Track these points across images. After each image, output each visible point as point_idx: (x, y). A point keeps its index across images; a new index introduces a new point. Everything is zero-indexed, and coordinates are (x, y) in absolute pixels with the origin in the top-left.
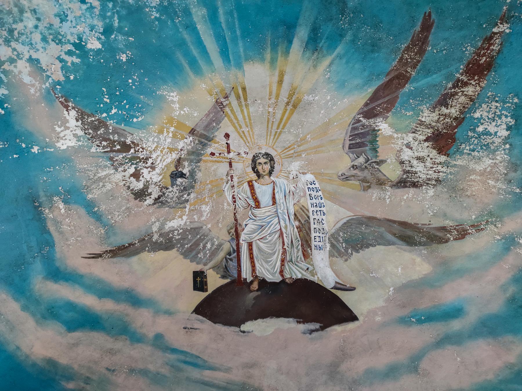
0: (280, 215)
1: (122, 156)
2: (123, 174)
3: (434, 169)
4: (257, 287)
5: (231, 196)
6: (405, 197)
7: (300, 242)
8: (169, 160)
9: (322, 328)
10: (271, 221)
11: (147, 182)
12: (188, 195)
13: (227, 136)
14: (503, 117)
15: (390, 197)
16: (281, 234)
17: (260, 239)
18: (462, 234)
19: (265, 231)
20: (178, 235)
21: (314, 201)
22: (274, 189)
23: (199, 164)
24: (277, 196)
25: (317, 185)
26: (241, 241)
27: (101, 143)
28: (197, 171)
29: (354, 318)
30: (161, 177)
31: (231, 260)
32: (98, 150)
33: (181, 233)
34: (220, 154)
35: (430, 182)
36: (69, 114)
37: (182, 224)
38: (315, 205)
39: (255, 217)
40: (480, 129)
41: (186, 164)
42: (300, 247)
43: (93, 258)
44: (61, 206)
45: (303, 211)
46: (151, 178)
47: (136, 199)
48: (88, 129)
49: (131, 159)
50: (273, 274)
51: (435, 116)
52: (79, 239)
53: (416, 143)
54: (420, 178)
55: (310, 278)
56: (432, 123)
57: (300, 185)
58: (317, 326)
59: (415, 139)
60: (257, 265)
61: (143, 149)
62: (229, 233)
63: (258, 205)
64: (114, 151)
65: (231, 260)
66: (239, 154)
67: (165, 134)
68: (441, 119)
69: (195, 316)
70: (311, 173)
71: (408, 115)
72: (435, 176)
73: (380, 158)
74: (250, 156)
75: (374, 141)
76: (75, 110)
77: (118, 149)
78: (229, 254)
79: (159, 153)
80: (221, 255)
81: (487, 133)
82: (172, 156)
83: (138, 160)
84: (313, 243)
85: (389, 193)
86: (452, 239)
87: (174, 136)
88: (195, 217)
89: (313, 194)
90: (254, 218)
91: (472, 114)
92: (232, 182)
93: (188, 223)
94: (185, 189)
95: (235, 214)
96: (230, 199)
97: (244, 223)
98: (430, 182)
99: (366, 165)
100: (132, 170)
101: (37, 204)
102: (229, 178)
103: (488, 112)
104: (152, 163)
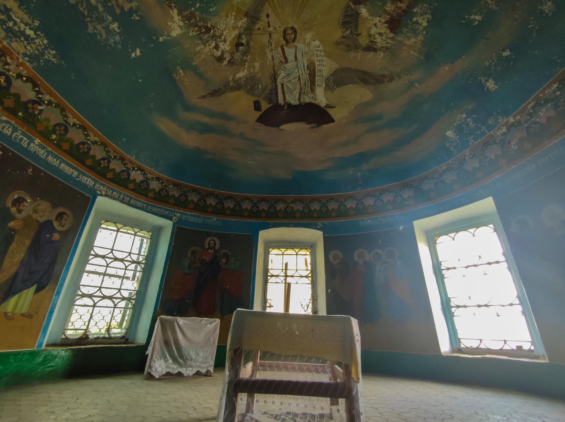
0: (299, 67)
1: (207, 36)
2: (209, 47)
3: (386, 41)
4: (287, 108)
5: (271, 57)
6: (368, 57)
7: (309, 83)
8: (233, 35)
9: (318, 126)
10: (294, 71)
11: (223, 51)
12: (246, 57)
13: (268, 16)
14: (427, 15)
15: (360, 57)
16: (299, 79)
17: (288, 81)
18: (391, 79)
19: (290, 77)
20: (243, 81)
21: (319, 58)
22: (296, 51)
23: (251, 36)
24: (298, 55)
25: (321, 48)
26: (278, 84)
27: (194, 29)
28: (251, 41)
29: (333, 121)
30: (230, 47)
31: (273, 94)
32: (193, 34)
33: (245, 80)
34: (264, 29)
35: (382, 49)
36: (173, 12)
37: (245, 75)
38: (319, 60)
39: (285, 68)
40: (414, 19)
41: (244, 37)
42: (309, 85)
43: (202, 98)
44: (181, 71)
45: (312, 64)
46: (225, 48)
47: (218, 62)
48: (185, 21)
49: (212, 37)
50: (295, 101)
51: (393, 7)
52: (194, 89)
53: (380, 24)
54: (378, 46)
55: (313, 102)
56: (391, 12)
57: (312, 48)
58: (316, 125)
59: (380, 21)
60: (287, 97)
61: (218, 29)
62: (271, 79)
63: (287, 61)
64: (202, 33)
65: (273, 94)
66: (275, 28)
67: (230, 17)
68: (396, 10)
69: (257, 123)
70: (318, 41)
71: (379, 4)
72: (386, 45)
73: (359, 32)
74: (282, 29)
75: (357, 20)
76: (176, 9)
77: (204, 31)
78: (272, 91)
79: (227, 31)
80: (267, 91)
81: (417, 22)
82: (235, 32)
83: (216, 38)
84: (317, 83)
85: (360, 54)
86: (386, 82)
87: (235, 19)
88: (251, 70)
89: (319, 53)
90: (284, 69)
91: (412, 9)
92: (271, 47)
93: (248, 74)
94: (245, 53)
95: (273, 67)
96: (270, 58)
97: (279, 72)
98: (382, 49)
99: (350, 36)
100: (214, 44)
101: (169, 72)
102: (270, 44)
103: (421, 9)
104: (224, 38)
